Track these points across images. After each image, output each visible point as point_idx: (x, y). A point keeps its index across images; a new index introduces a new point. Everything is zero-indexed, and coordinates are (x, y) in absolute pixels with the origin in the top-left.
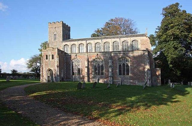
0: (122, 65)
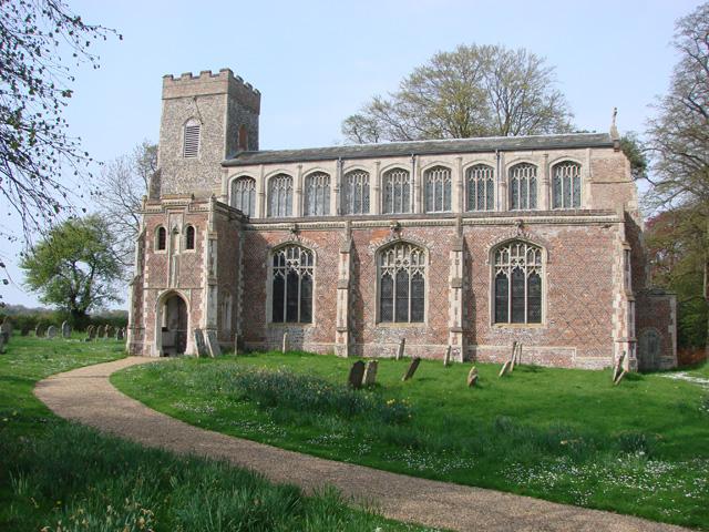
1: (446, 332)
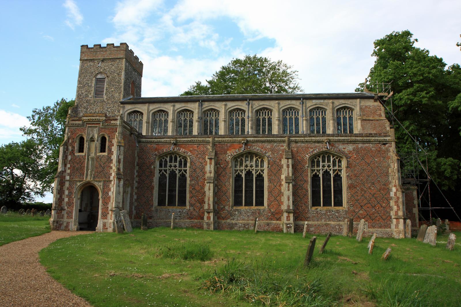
0: (321, 176)
1: (281, 213)
